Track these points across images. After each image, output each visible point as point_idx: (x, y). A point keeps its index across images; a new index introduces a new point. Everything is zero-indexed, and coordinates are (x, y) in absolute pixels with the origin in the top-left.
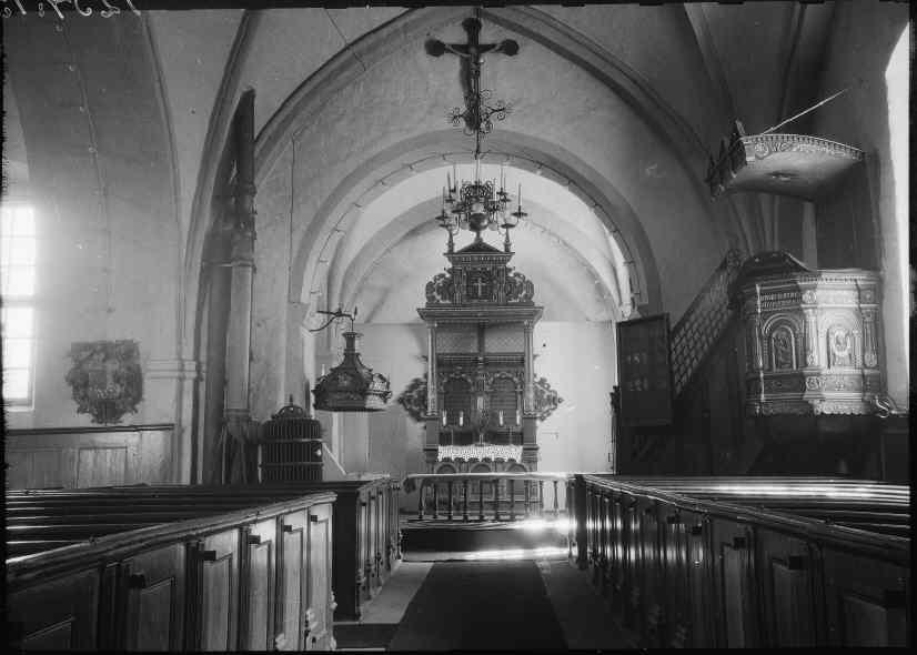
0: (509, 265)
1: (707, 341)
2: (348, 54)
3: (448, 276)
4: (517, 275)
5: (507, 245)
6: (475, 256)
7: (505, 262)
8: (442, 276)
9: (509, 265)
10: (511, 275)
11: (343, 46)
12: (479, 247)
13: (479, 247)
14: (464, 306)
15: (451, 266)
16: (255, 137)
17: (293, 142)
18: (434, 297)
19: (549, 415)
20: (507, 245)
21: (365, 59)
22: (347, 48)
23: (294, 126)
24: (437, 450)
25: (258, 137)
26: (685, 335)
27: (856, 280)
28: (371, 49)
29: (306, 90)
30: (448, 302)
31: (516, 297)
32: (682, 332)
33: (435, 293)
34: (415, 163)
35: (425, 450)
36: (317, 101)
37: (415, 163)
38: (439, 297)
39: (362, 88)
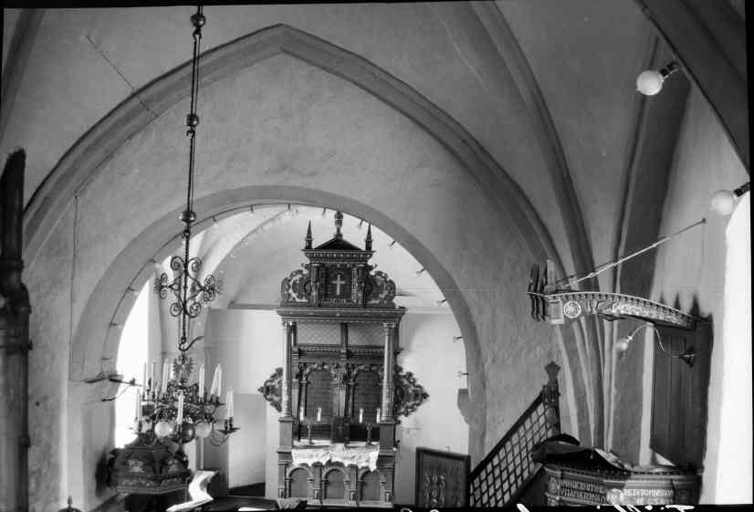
0: (370, 262)
1: (516, 482)
2: (135, 102)
3: (305, 272)
4: (379, 273)
5: (369, 242)
6: (329, 253)
7: (365, 260)
8: (301, 272)
9: (370, 262)
10: (372, 273)
11: (129, 92)
12: (337, 244)
13: (337, 244)
14: (320, 306)
15: (308, 263)
16: (24, 206)
17: (76, 197)
18: (289, 295)
19: (414, 410)
20: (369, 242)
21: (155, 108)
22: (134, 95)
23: (73, 182)
24: (290, 453)
25: (27, 208)
26: (499, 465)
27: (672, 480)
28: (161, 96)
29: (86, 143)
30: (304, 300)
31: (376, 298)
32: (483, 475)
33: (291, 291)
34: (217, 215)
35: (279, 453)
36: (98, 155)
37: (217, 215)
38: (294, 295)
39: (153, 137)
